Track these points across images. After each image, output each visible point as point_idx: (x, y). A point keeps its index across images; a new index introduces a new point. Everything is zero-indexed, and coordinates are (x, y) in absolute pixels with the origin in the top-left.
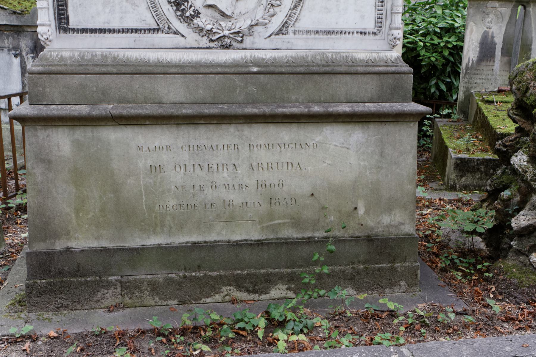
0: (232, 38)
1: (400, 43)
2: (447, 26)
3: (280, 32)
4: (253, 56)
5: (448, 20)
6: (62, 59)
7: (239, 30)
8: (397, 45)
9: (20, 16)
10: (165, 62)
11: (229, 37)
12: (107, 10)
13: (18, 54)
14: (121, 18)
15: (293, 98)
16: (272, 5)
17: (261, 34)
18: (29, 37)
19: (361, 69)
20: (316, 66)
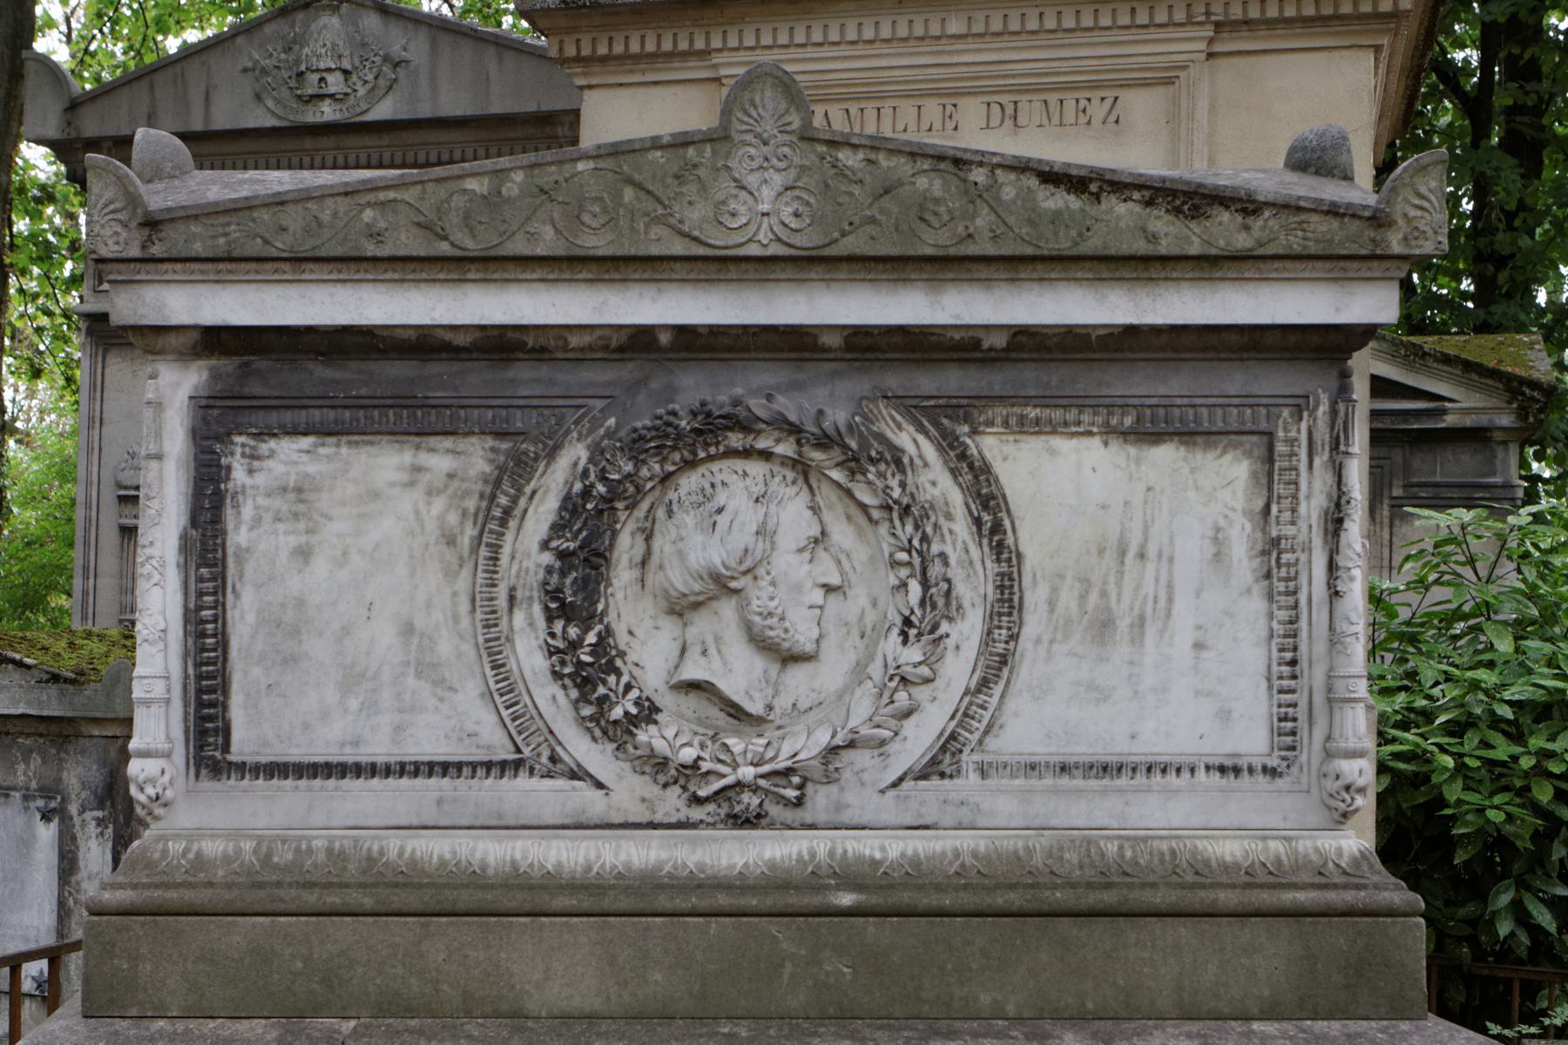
0: (767, 792)
1: (1366, 804)
2: (1540, 695)
3: (936, 766)
4: (840, 851)
5: (1542, 676)
6: (200, 862)
7: (789, 763)
8: (1357, 810)
9: (71, 688)
10: (536, 873)
11: (755, 789)
12: (354, 704)
13: (54, 810)
14: (398, 729)
15: (985, 999)
16: (903, 679)
17: (866, 777)
18: (94, 757)
19: (1227, 898)
20: (1063, 886)
